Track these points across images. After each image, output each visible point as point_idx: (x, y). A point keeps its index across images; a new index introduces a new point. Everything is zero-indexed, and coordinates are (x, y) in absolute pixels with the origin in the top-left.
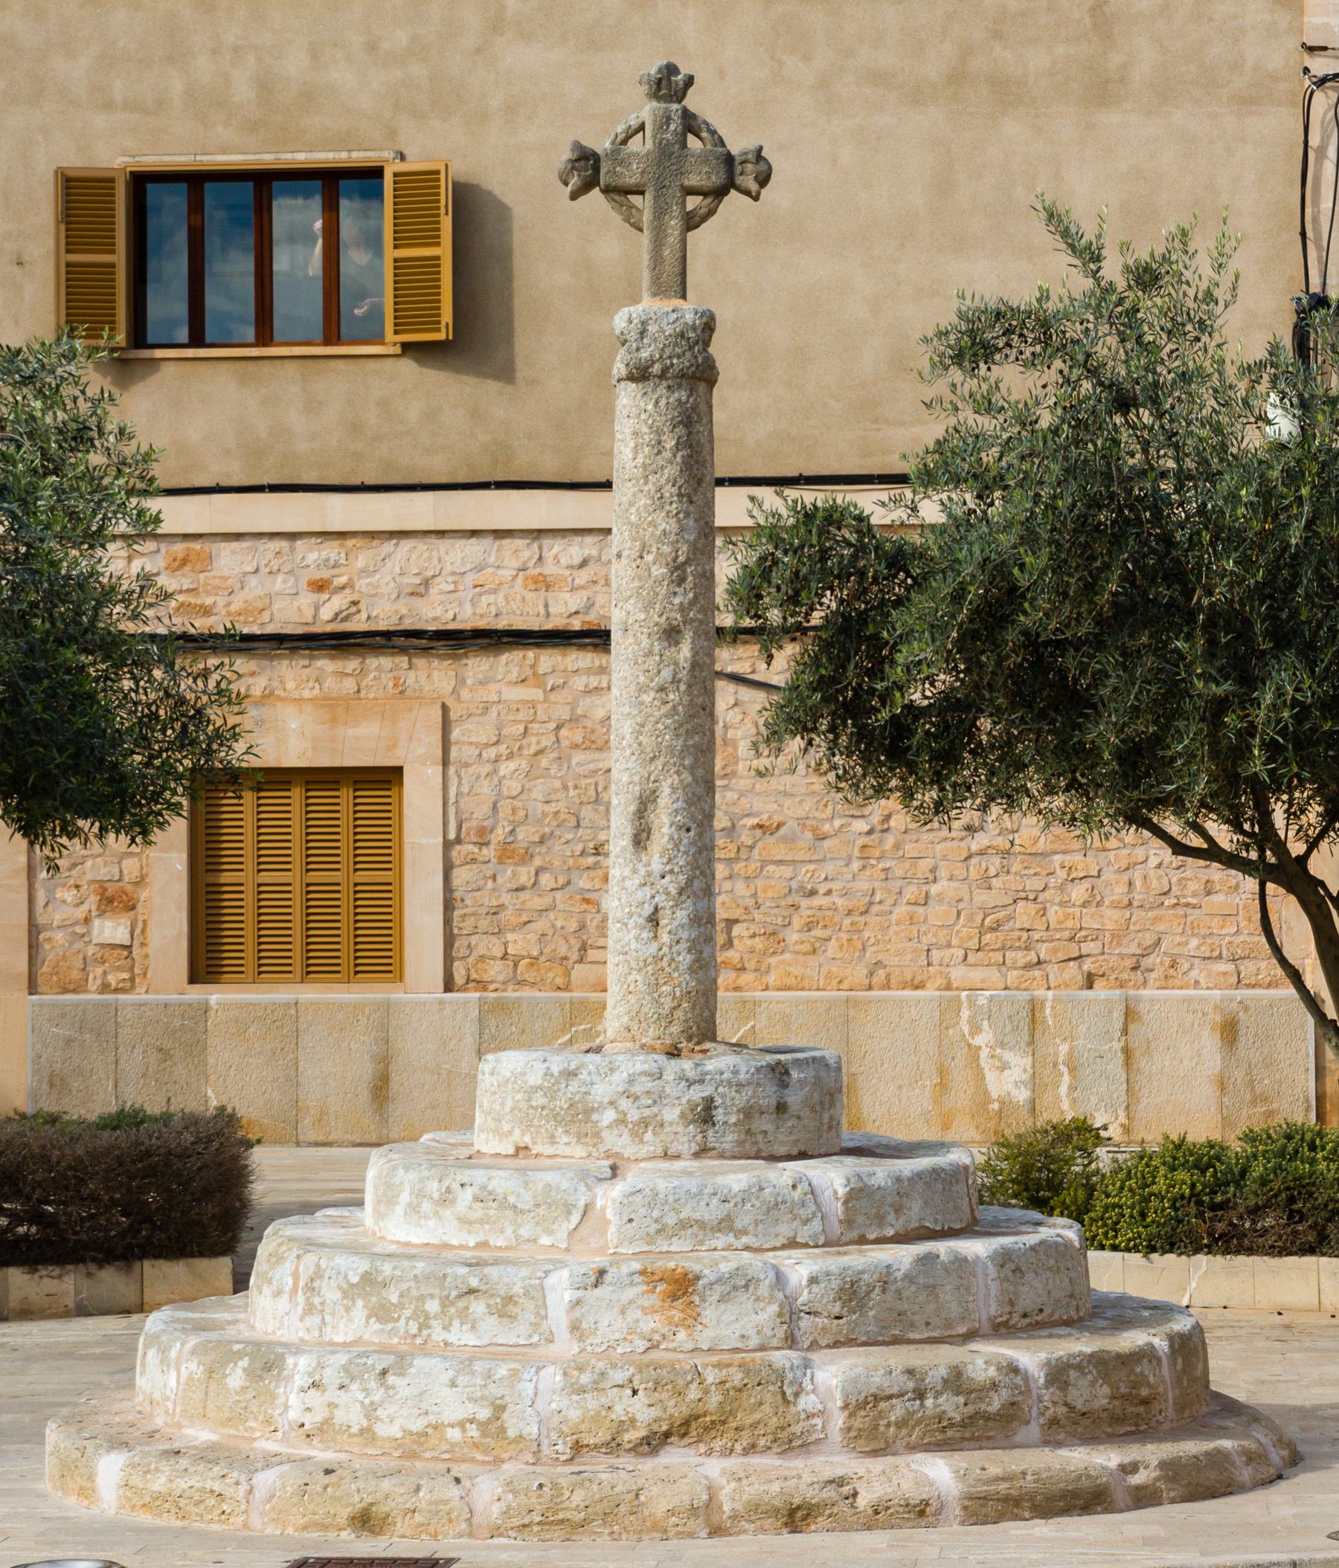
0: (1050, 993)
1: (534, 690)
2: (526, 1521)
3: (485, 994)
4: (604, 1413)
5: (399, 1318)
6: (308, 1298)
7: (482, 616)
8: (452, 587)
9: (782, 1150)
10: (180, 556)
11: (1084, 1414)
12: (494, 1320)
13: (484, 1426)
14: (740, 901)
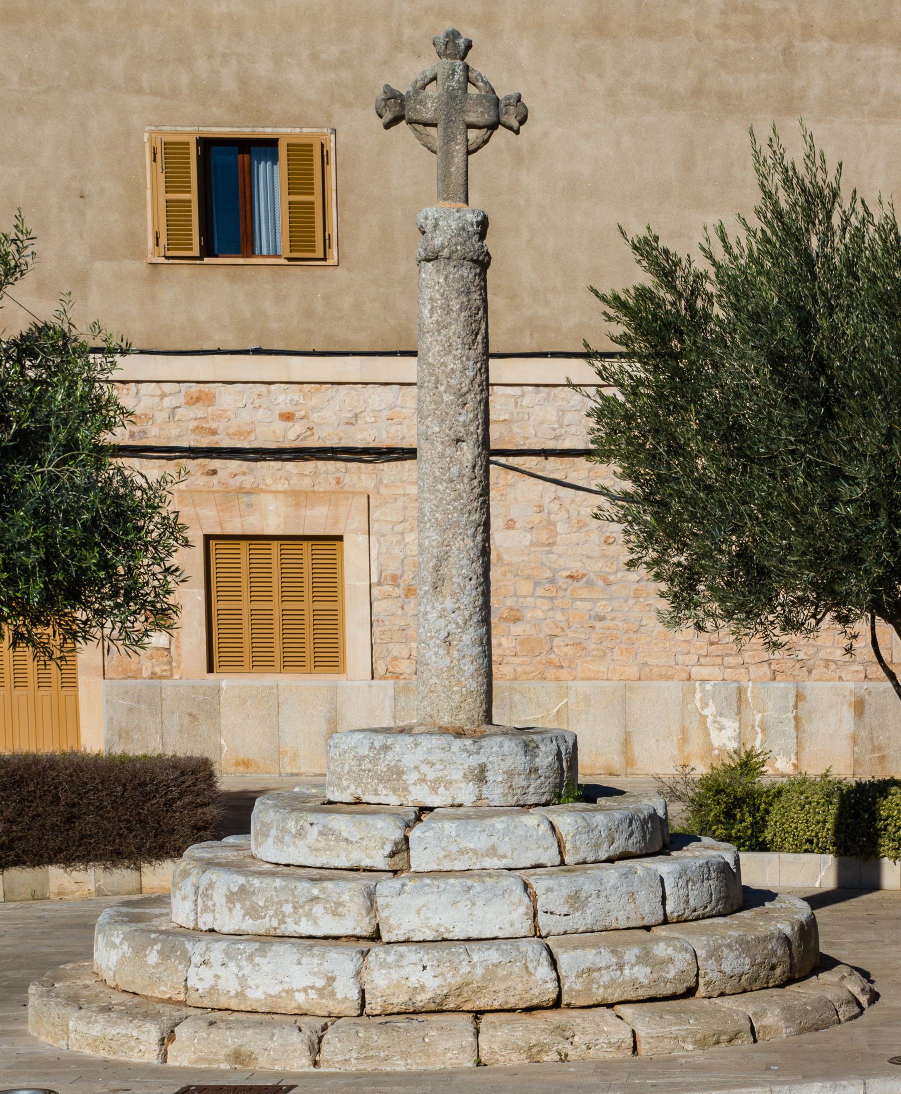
2: (347, 1057)
4: (403, 982)
5: (265, 916)
7: (392, 438)
8: (373, 420)
9: (532, 800)
10: (195, 395)
12: (329, 917)
13: (320, 991)
14: (558, 624)
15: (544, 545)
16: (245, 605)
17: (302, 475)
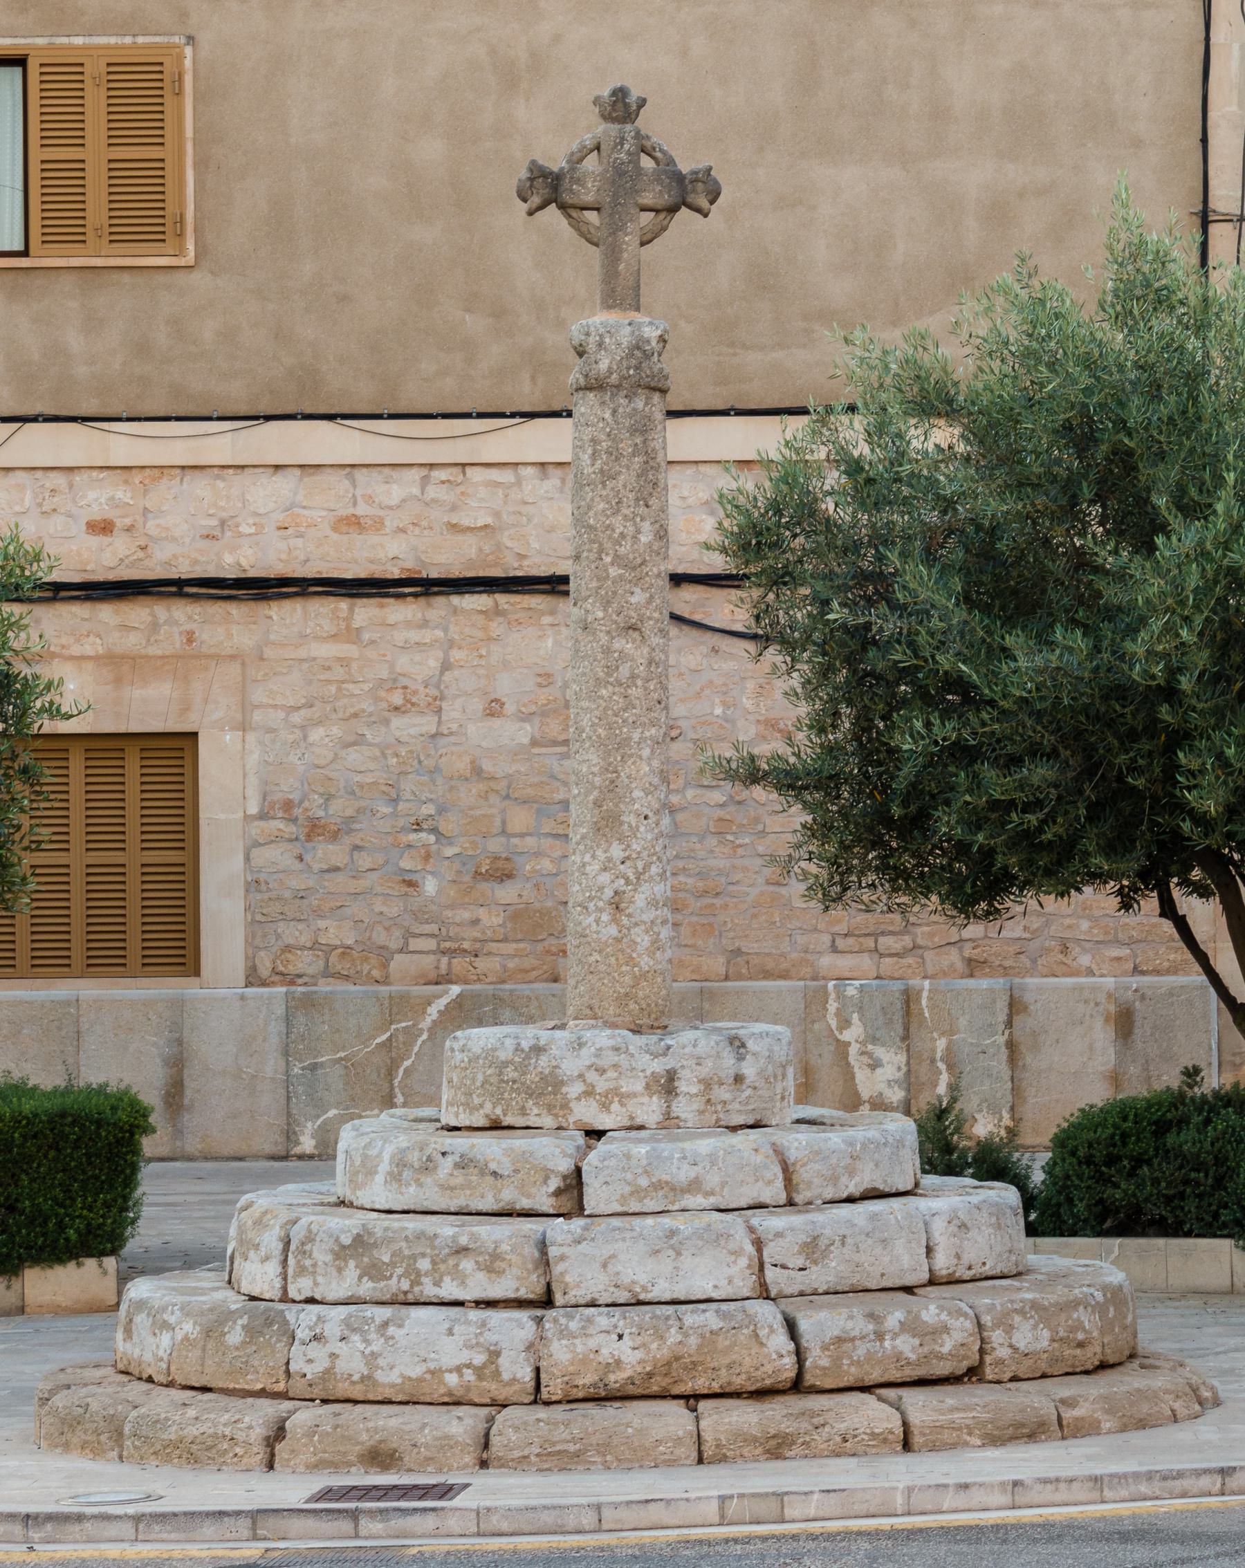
0: (927, 983)
1: (346, 646)
3: (293, 988)
4: (592, 1356)
5: (391, 1276)
6: (299, 1261)
8: (253, 530)
11: (1026, 1355)
12: (481, 1276)
13: (479, 1371)
15: (555, 743)
16: (77, 858)
17: (125, 628)
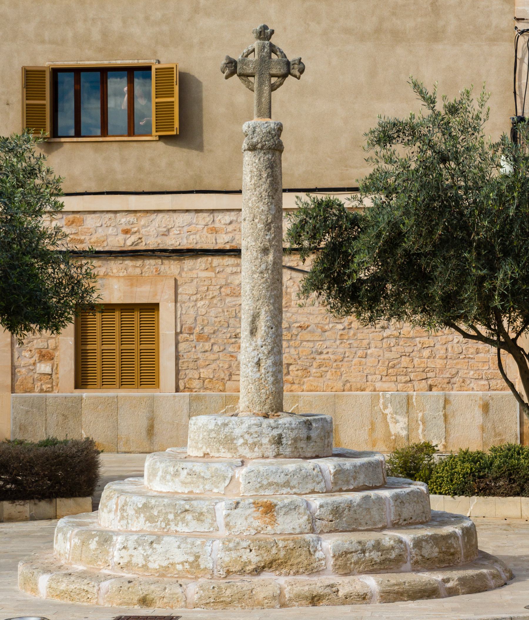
0: (415, 393)
1: (211, 273)
3: (192, 393)
4: (238, 559)
5: (158, 521)
7: (190, 244)
8: (178, 232)
9: (309, 455)
10: (71, 220)
11: (428, 559)
12: (195, 522)
13: (191, 564)
